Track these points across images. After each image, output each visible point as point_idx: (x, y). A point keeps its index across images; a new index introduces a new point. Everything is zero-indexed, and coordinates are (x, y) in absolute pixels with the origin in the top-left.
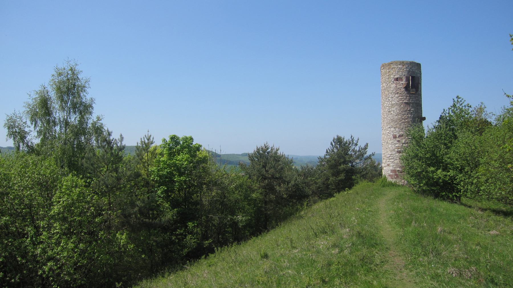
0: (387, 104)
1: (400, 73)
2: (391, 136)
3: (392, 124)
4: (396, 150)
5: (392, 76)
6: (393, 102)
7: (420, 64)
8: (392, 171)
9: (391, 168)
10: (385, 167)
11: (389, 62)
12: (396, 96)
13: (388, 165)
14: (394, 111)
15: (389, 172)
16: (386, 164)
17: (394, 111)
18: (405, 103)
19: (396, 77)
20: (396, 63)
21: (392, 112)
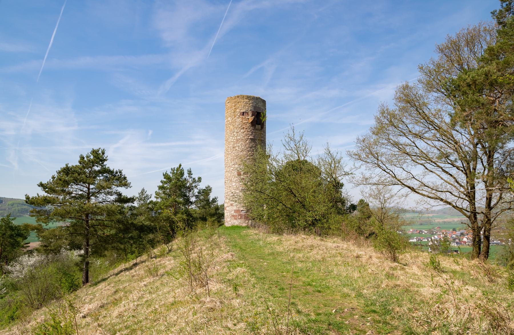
0: (231, 139)
1: (247, 107)
2: (236, 173)
3: (236, 161)
4: (241, 188)
5: (238, 110)
6: (239, 138)
7: (265, 101)
8: (236, 211)
9: (235, 208)
10: (229, 207)
11: (236, 96)
12: (242, 131)
13: (232, 205)
14: (239, 147)
15: (233, 212)
16: (229, 204)
17: (239, 147)
18: (250, 139)
19: (242, 111)
20: (243, 97)
21: (237, 148)
